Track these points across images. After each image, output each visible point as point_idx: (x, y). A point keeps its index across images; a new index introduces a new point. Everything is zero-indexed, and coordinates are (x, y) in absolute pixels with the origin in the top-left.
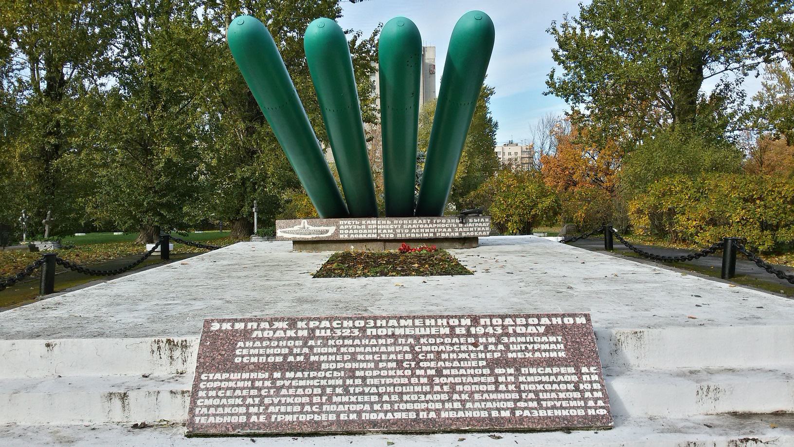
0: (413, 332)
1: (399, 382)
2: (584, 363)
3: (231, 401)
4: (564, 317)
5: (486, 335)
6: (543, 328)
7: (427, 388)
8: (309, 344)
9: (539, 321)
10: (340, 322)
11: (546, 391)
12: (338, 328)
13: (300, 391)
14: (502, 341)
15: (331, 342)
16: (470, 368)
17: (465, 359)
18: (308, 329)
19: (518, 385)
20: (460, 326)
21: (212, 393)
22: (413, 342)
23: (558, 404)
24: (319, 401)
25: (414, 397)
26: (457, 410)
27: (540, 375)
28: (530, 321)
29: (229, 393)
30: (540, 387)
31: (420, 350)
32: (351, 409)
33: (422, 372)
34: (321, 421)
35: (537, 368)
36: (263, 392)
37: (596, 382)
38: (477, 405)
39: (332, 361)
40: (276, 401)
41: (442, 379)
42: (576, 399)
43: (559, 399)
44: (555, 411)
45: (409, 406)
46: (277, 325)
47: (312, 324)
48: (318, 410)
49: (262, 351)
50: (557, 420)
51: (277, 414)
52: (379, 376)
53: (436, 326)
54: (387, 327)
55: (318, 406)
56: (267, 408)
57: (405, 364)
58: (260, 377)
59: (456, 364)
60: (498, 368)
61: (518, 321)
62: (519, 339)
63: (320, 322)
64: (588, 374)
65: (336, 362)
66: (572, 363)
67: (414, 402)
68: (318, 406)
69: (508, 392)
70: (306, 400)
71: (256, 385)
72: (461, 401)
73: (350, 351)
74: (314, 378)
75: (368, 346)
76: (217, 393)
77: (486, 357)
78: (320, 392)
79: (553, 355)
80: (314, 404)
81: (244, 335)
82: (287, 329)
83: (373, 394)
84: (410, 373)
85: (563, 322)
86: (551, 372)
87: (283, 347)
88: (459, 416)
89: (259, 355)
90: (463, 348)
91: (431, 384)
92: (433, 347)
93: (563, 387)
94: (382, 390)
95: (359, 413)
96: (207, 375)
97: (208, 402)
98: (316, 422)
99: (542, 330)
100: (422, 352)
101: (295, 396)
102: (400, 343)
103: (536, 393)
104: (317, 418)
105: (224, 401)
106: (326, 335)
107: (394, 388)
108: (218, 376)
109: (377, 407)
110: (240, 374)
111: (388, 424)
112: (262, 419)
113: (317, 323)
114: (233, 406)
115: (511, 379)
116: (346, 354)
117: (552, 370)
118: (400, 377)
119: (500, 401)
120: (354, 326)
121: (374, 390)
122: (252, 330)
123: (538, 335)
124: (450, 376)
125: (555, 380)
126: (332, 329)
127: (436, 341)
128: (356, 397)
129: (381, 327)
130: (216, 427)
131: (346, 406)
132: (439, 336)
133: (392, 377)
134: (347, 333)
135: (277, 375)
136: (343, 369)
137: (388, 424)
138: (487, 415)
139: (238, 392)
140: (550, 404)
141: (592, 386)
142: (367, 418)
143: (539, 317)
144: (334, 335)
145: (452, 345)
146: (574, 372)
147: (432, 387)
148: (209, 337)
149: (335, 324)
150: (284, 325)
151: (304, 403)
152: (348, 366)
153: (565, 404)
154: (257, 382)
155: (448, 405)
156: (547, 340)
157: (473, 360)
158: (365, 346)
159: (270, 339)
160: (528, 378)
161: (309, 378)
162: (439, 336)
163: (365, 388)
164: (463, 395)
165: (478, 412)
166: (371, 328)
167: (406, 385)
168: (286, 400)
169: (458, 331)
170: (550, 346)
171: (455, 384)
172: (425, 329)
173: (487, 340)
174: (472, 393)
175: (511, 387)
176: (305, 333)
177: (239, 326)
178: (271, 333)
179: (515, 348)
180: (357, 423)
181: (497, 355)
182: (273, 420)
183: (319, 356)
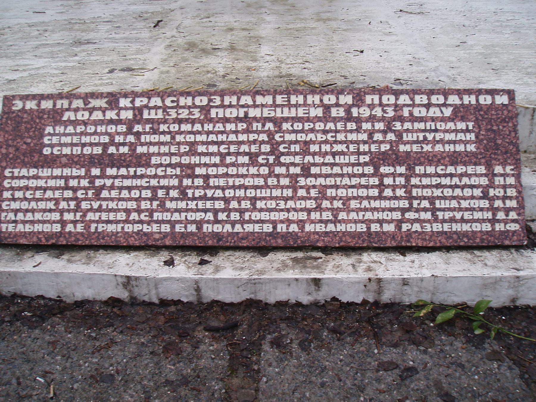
0: (273, 114)
1: (251, 184)
2: (499, 160)
3: (42, 205)
4: (480, 94)
5: (372, 119)
6: (450, 109)
7: (289, 193)
8: (135, 130)
9: (446, 99)
10: (175, 99)
11: (445, 198)
12: (172, 108)
13: (125, 194)
14: (393, 128)
15: (163, 127)
16: (347, 165)
17: (342, 153)
18: (133, 108)
19: (409, 188)
20: (337, 105)
21: (19, 194)
22: (272, 128)
23: (458, 216)
24: (149, 207)
25: (272, 204)
26: (326, 222)
27: (439, 176)
28: (434, 99)
29: (38, 194)
30: (438, 192)
31: (286, 150)
32: (189, 218)
33: (282, 170)
34: (152, 233)
35: (437, 166)
36: (80, 194)
37: (511, 186)
38: (353, 216)
39: (165, 154)
40: (96, 205)
41: (309, 179)
42: (482, 210)
43: (460, 209)
44: (454, 225)
45: (264, 216)
46: (95, 103)
47: (138, 102)
48: (147, 218)
49: (75, 140)
50: (455, 236)
51: (97, 222)
52: (226, 175)
53: (305, 104)
54: (239, 106)
55: (147, 214)
56: (84, 215)
57: (260, 160)
58: (74, 174)
59: (329, 159)
60: (385, 166)
61: (418, 99)
62: (417, 126)
63: (149, 98)
64: (501, 175)
65: (171, 154)
66: (483, 161)
67: (270, 210)
68: (147, 214)
69: (396, 198)
70: (132, 205)
71: (71, 185)
72: (332, 209)
73: (188, 140)
74: (142, 176)
75: (212, 132)
76: (24, 194)
77: (370, 149)
78: (150, 195)
79: (460, 148)
80: (143, 211)
81: (53, 118)
82: (106, 109)
83: (218, 199)
84: (267, 172)
85: (477, 101)
86: (454, 172)
87: (102, 134)
88: (328, 230)
89: (72, 145)
90: (340, 137)
91: (294, 187)
92: (299, 135)
93: (468, 192)
94: (229, 193)
95: (199, 224)
96: (11, 170)
97: (15, 205)
98: (146, 234)
99: (448, 112)
100: (283, 142)
101: (120, 199)
102: (255, 129)
103: (432, 200)
104: (146, 228)
105: (33, 204)
106: (156, 117)
107: (245, 192)
108: (24, 172)
109: (222, 216)
110: (50, 170)
111: (236, 239)
112: (80, 228)
113: (145, 101)
114: (45, 211)
115: (401, 181)
116: (183, 144)
117: (456, 169)
118: (253, 176)
119: (383, 210)
120: (194, 104)
121: (219, 193)
122: (63, 111)
123: (443, 119)
124: (320, 175)
125: (458, 183)
126: (165, 109)
127: (303, 127)
128: (195, 202)
129: (230, 106)
130: (26, 237)
131: (183, 215)
132: (308, 120)
133: (243, 176)
134: (184, 114)
135: (96, 172)
136: (179, 165)
137: (236, 239)
138: (365, 230)
139: (49, 194)
140: (448, 215)
141: (505, 192)
142: (210, 230)
143: (446, 93)
144: (167, 117)
145: (325, 132)
146: (484, 172)
147: (295, 191)
148: (11, 119)
149: (168, 102)
150: (101, 103)
151: (129, 210)
152: (185, 160)
153: (467, 215)
154: (71, 180)
155: (315, 216)
156: (453, 128)
157: (352, 153)
158: (208, 133)
159: (85, 123)
160: (424, 179)
161: (135, 176)
162: (308, 120)
163: (207, 191)
164: (335, 202)
165: (353, 225)
166: (217, 107)
167: (261, 187)
168: (107, 205)
169: (334, 112)
170: (456, 135)
171: (350, 199)
172: (290, 109)
173: (373, 126)
174: (346, 200)
175: (400, 192)
176: (128, 115)
177: (47, 105)
178: (87, 114)
179: (410, 138)
180: (197, 236)
181: (385, 147)
182: (93, 229)
183: (148, 147)
